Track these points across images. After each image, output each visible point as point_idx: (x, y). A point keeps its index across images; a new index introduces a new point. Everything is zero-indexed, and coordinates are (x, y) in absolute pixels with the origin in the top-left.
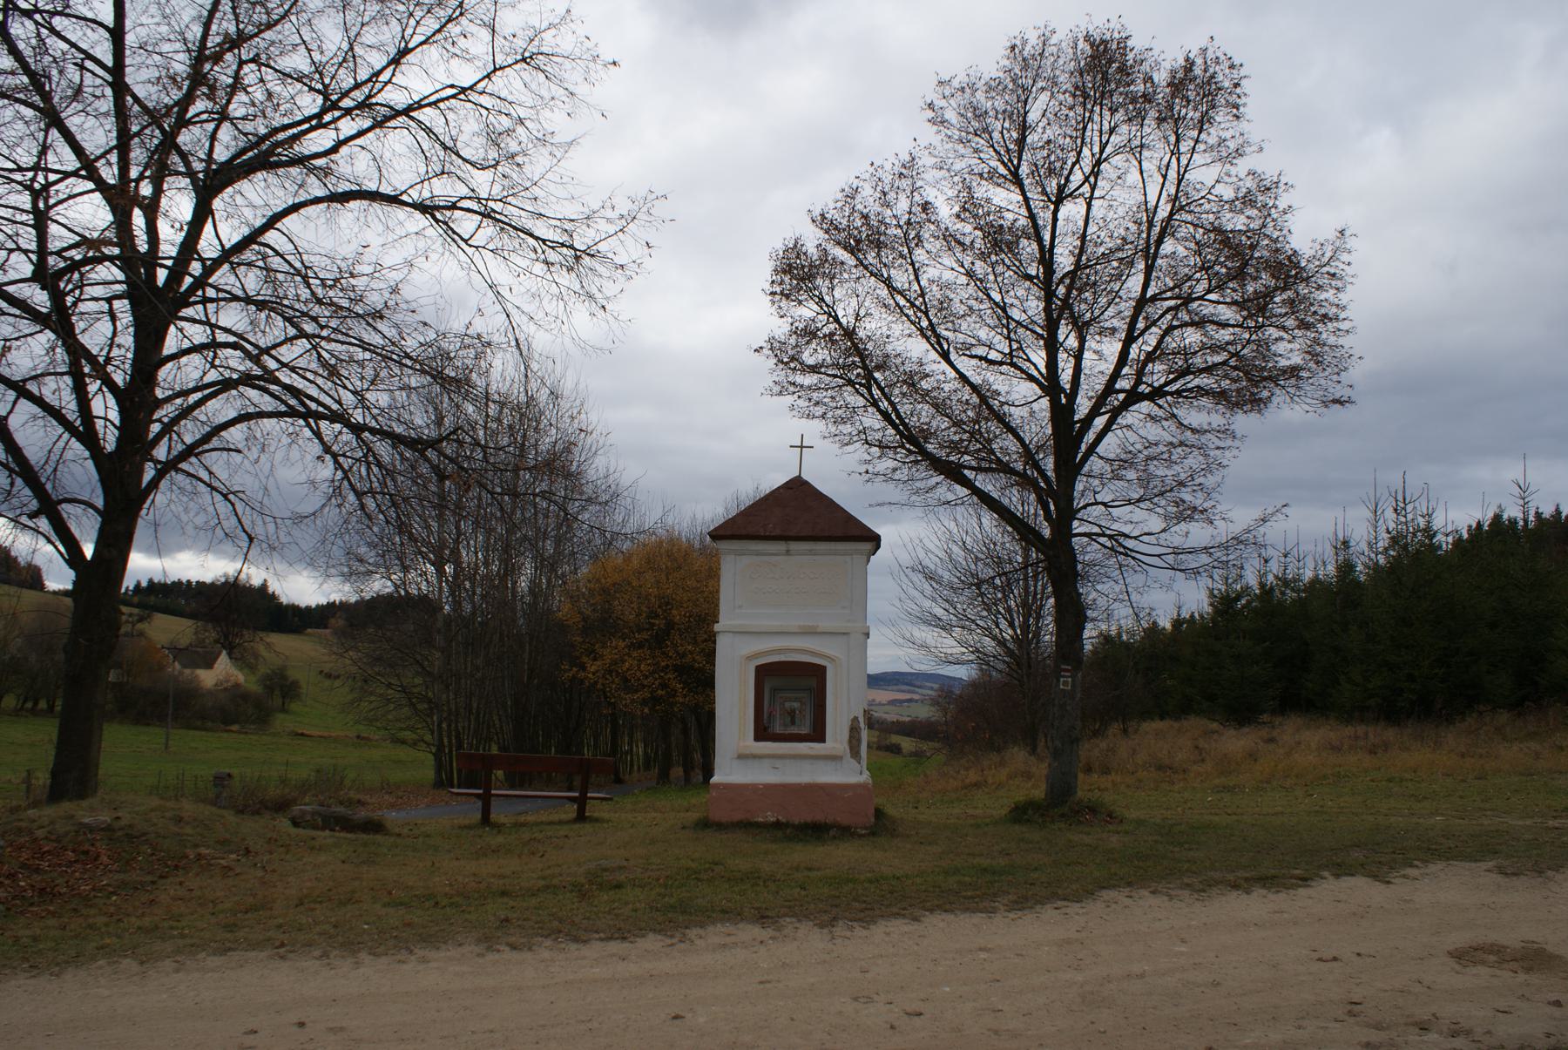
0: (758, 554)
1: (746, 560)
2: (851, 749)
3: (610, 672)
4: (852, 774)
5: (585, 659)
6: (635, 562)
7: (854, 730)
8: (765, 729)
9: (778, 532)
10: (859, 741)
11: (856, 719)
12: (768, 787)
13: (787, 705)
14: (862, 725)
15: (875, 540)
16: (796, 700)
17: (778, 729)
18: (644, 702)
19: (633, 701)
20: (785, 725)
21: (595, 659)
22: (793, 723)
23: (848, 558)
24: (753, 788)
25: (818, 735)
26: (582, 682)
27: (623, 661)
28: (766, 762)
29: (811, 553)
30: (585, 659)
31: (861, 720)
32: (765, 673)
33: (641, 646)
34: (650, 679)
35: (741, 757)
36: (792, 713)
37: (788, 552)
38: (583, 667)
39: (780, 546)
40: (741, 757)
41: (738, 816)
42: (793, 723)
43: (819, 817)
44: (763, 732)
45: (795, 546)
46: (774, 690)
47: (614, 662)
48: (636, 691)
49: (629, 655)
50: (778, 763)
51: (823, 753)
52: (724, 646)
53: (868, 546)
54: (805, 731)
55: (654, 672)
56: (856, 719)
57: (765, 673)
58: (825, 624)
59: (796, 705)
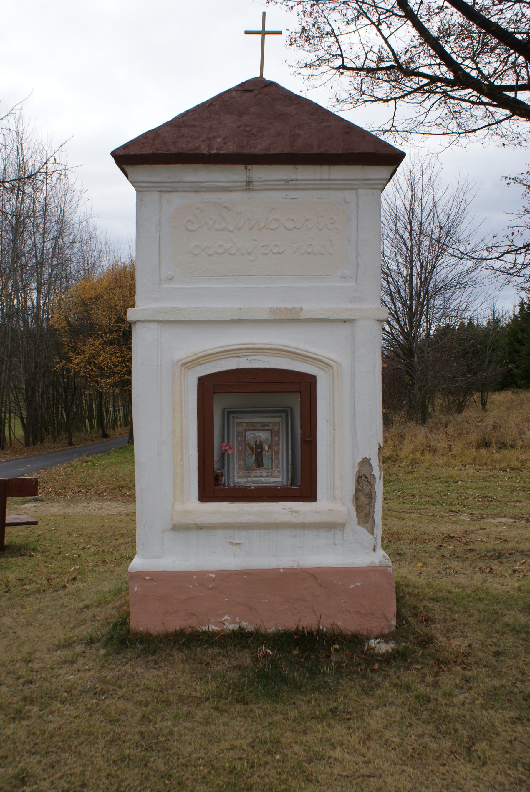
0: (197, 189)
1: (177, 200)
2: (359, 508)
3: (90, 364)
4: (359, 551)
5: (71, 354)
6: (105, 283)
7: (363, 479)
8: (217, 478)
9: (231, 148)
10: (371, 497)
11: (366, 461)
12: (226, 577)
13: (250, 436)
14: (377, 472)
15: (393, 158)
16: (264, 428)
17: (237, 478)
18: (115, 385)
19: (107, 384)
20: (248, 469)
21: (78, 354)
22: (259, 464)
23: (349, 195)
24: (199, 578)
25: (302, 486)
26: (68, 370)
27: (99, 355)
28: (220, 533)
29: (289, 185)
30: (71, 354)
31: (375, 463)
32: (212, 388)
33: (111, 343)
34: (119, 368)
35: (177, 528)
36: (257, 450)
37: (249, 186)
38: (70, 360)
39: (236, 174)
40: (177, 528)
41: (175, 624)
42: (259, 464)
43: (308, 622)
44: (212, 486)
45: (261, 173)
46: (229, 413)
47: (92, 356)
48: (109, 377)
49: (103, 350)
50: (240, 536)
51: (316, 519)
52: (142, 342)
53: (376, 172)
54: (277, 478)
55: (122, 362)
56: (366, 461)
57: (212, 388)
58: (312, 307)
59: (264, 436)
